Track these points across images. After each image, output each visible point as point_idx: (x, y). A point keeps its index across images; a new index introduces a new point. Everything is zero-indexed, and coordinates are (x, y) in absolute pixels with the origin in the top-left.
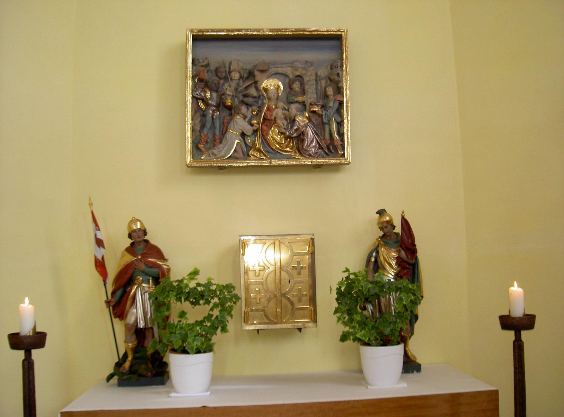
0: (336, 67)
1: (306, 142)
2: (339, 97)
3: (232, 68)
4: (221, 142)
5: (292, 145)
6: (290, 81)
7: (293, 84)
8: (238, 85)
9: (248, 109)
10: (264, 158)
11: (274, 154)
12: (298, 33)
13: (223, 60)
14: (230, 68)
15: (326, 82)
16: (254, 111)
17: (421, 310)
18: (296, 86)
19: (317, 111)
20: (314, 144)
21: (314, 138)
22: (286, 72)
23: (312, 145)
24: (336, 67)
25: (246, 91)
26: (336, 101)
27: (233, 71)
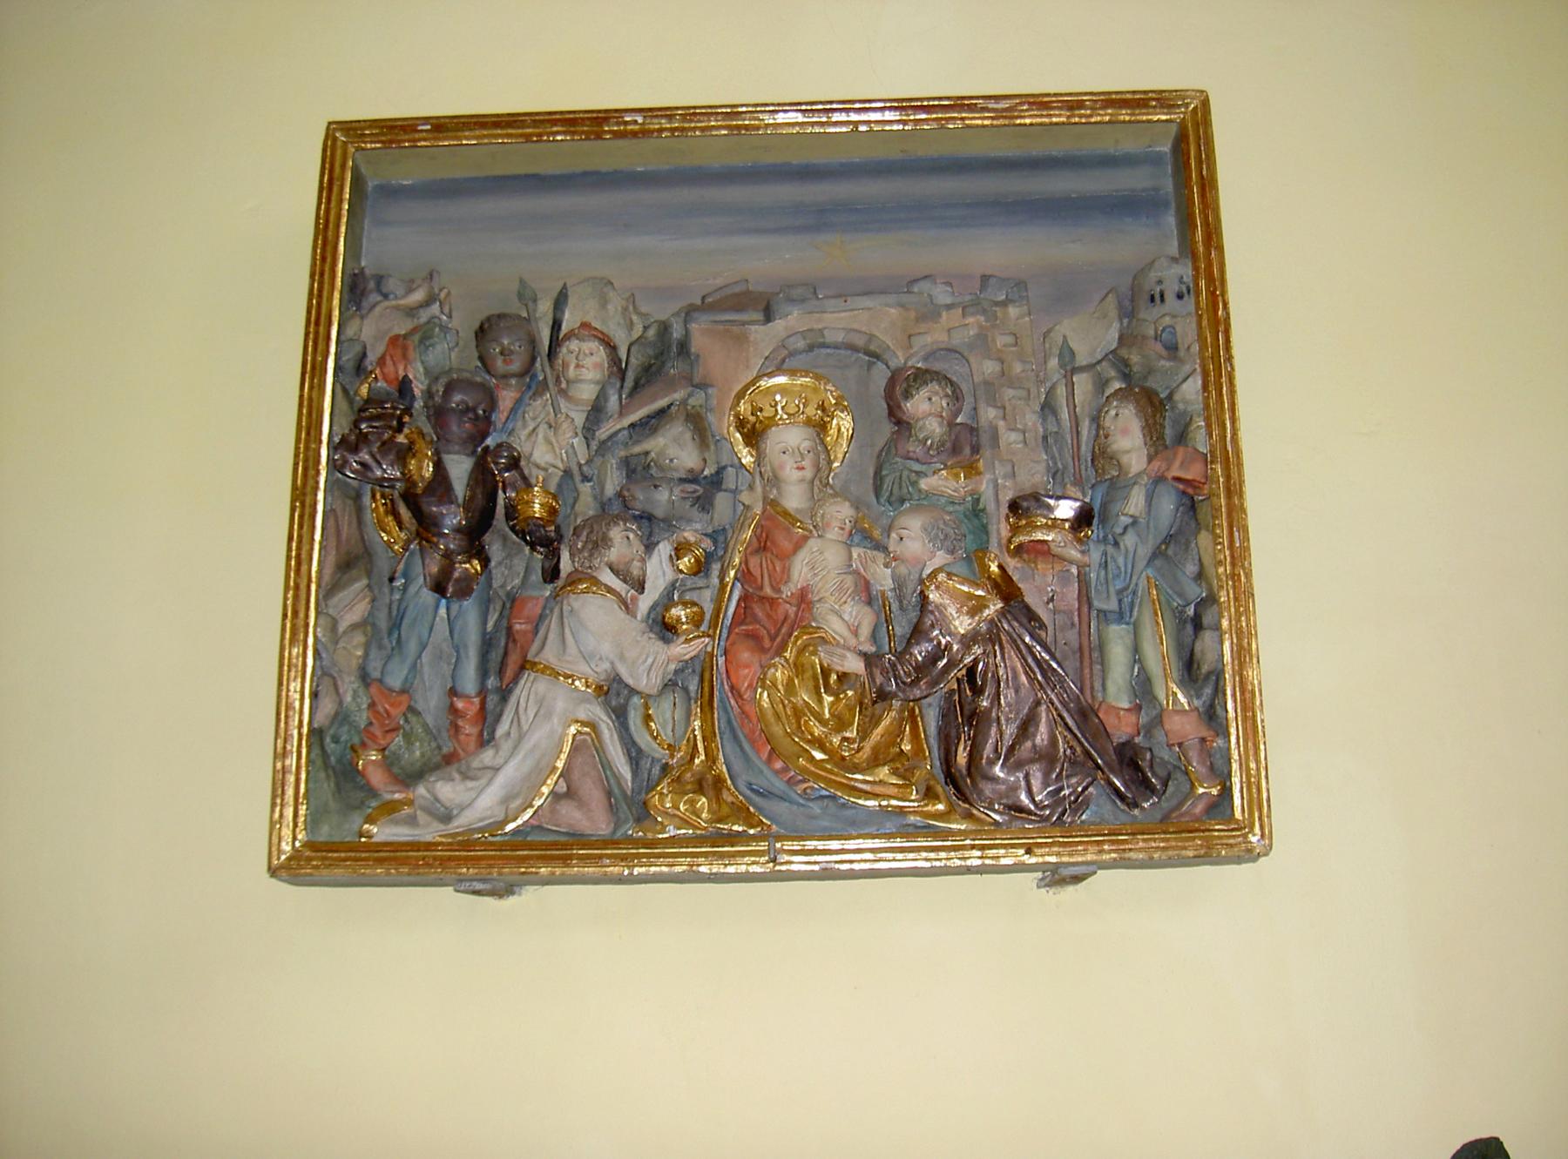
0: (1152, 299)
1: (994, 730)
2: (1177, 463)
3: (569, 321)
4: (486, 740)
5: (907, 747)
6: (892, 382)
7: (907, 395)
8: (596, 412)
9: (650, 547)
10: (1110, 536)
11: (803, 805)
12: (934, 116)
13: (522, 281)
14: (556, 325)
15: (1102, 384)
16: (1220, 550)
17: (1263, 859)
18: (924, 406)
19: (1052, 546)
20: (1038, 740)
21: (1038, 703)
22: (871, 337)
23: (1028, 744)
24: (1152, 299)
25: (638, 442)
26: (1161, 488)
27: (569, 336)
